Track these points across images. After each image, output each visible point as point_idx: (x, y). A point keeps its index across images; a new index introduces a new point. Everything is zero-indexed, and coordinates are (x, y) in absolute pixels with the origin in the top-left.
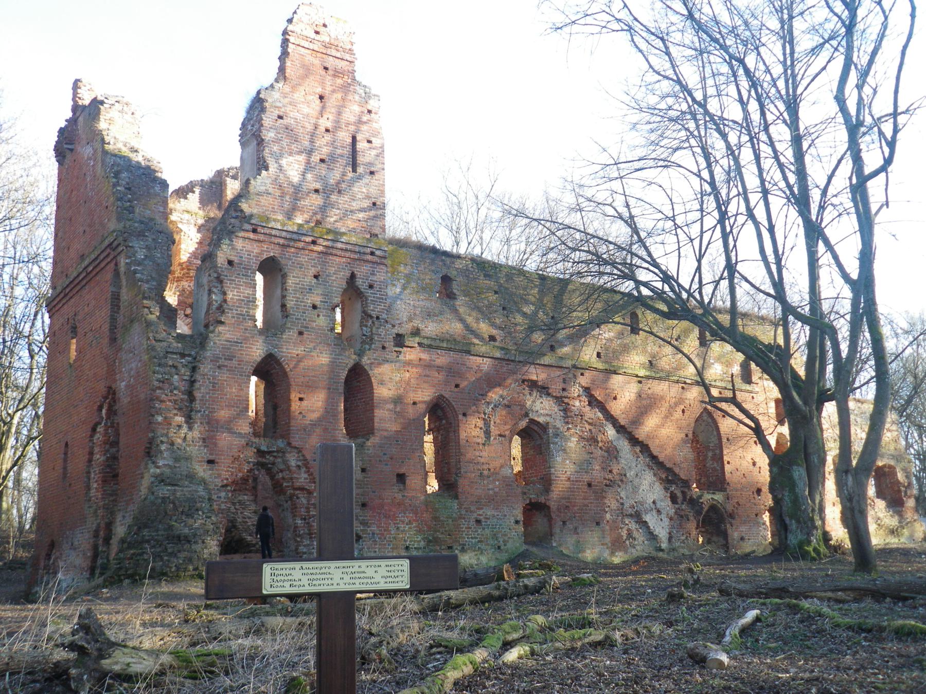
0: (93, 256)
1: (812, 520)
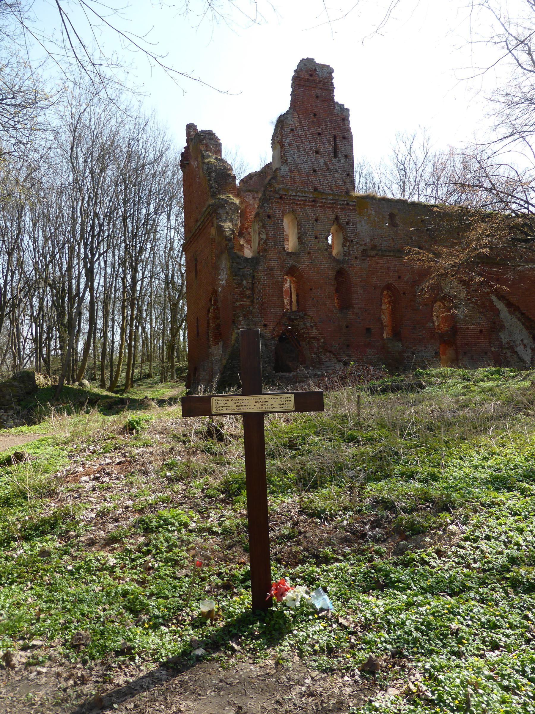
0: (201, 220)
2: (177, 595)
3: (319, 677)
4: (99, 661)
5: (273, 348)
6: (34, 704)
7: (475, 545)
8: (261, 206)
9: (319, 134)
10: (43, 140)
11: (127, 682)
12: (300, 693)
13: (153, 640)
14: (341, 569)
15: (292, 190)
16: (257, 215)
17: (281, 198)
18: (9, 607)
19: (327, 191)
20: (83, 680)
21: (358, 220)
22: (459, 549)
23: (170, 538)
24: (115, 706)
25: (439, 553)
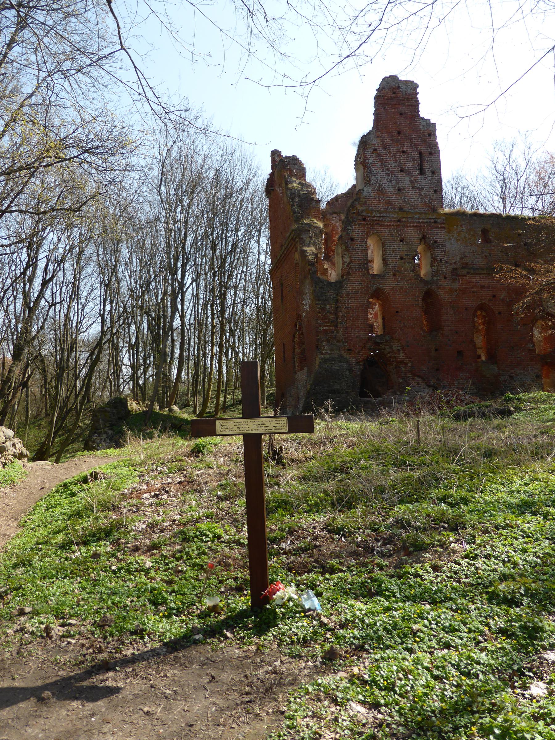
2: (195, 593)
3: (287, 661)
4: (116, 638)
5: (359, 373)
6: (59, 663)
7: (472, 562)
8: (344, 229)
9: (404, 152)
10: (132, 180)
11: (133, 654)
12: (267, 671)
13: (164, 625)
14: (341, 579)
15: (375, 211)
16: (341, 238)
17: (364, 220)
18: (59, 595)
19: (413, 210)
20: (100, 650)
21: (447, 237)
22: (454, 565)
23: (201, 547)
24: (117, 668)
25: (436, 568)
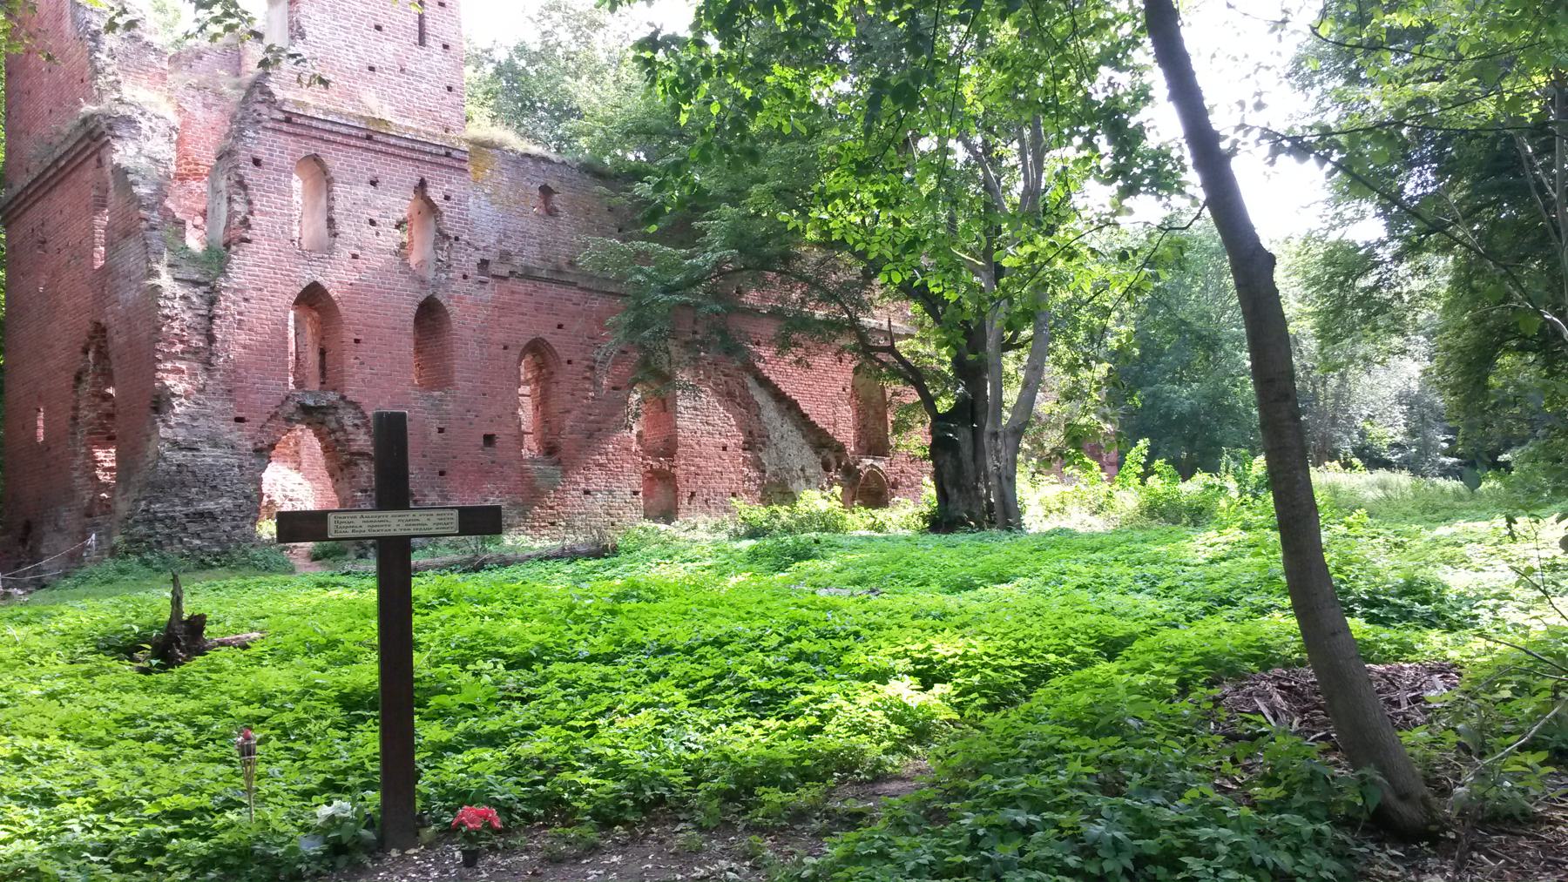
1: (976, 488)
